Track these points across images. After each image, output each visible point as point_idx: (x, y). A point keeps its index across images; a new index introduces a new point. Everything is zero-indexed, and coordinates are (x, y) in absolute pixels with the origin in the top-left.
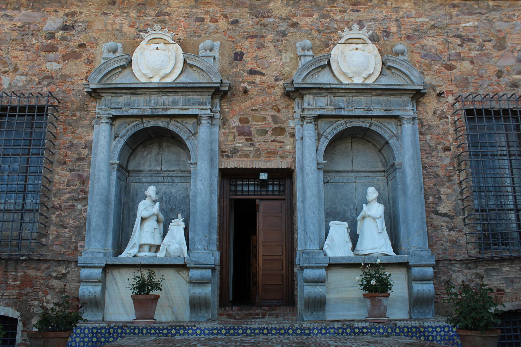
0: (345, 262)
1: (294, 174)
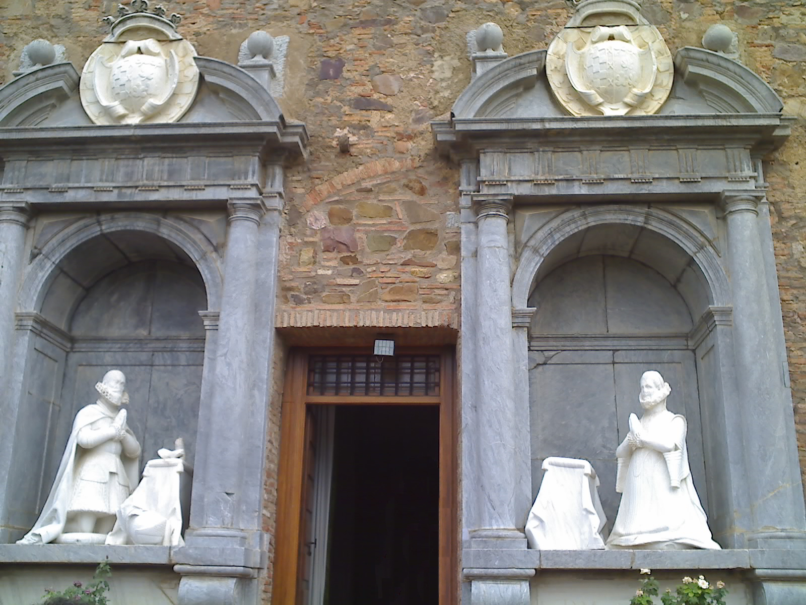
0: (581, 564)
1: (459, 340)
